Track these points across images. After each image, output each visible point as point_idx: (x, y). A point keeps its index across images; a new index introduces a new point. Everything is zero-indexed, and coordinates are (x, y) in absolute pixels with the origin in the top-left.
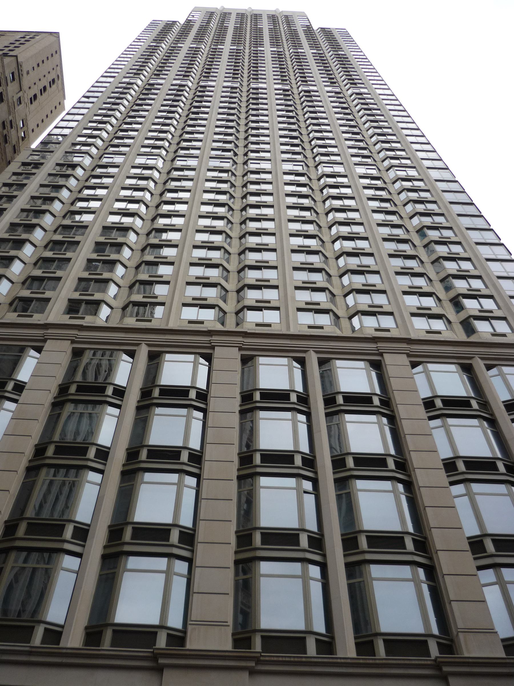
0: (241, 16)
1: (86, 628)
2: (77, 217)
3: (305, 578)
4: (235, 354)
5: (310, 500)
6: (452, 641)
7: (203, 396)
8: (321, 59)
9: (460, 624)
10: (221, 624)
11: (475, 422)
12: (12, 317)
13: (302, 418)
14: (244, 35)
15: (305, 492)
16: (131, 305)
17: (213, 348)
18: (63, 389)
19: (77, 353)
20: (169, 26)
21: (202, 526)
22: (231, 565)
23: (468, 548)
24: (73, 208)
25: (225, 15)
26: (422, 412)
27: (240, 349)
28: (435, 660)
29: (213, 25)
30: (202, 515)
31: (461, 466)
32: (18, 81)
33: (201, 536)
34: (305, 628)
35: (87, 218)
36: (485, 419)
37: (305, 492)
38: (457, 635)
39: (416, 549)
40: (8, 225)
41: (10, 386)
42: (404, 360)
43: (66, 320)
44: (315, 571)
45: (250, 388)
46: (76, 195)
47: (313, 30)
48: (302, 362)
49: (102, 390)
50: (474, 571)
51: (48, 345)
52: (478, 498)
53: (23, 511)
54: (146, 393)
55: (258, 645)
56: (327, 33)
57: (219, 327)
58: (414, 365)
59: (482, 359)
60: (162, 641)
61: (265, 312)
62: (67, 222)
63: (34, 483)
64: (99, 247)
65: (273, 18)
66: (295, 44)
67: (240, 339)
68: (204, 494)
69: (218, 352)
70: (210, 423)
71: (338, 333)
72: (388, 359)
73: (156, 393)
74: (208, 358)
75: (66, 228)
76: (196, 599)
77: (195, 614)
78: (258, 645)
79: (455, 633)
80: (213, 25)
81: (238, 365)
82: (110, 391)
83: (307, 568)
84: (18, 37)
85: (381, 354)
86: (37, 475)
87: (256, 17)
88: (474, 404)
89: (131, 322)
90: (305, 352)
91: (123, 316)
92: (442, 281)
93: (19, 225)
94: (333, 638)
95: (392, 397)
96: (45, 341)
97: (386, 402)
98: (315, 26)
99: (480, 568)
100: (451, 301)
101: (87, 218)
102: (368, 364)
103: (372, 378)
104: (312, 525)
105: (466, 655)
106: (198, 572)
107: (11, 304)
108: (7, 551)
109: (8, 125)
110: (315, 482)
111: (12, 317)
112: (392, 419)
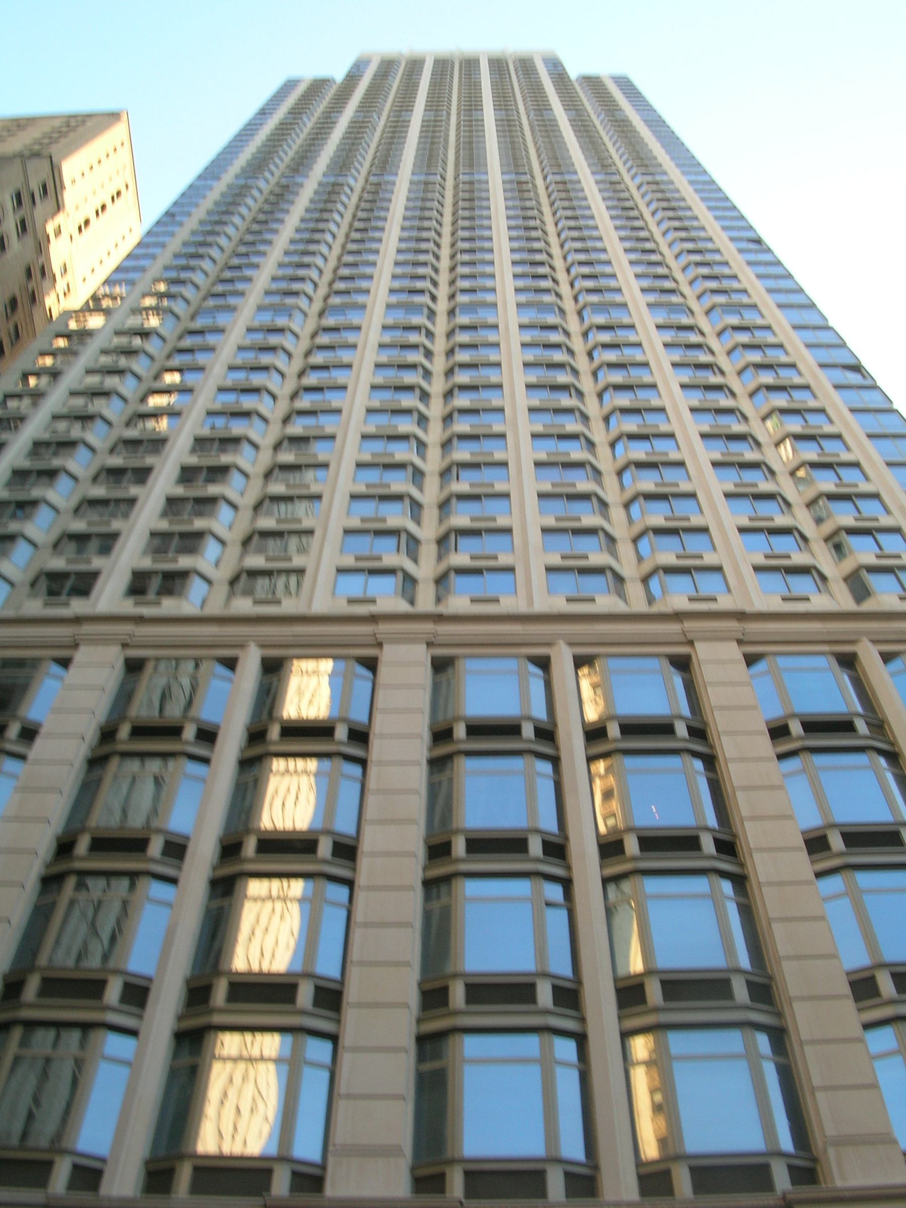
0: (443, 66)
1: (147, 1163)
2: (151, 424)
3: (547, 1064)
4: (421, 655)
5: (557, 919)
6: (815, 1160)
7: (360, 736)
8: (583, 128)
9: (830, 1130)
10: (389, 1151)
11: (861, 759)
12: (35, 607)
13: (546, 767)
14: (446, 103)
15: (548, 904)
16: (244, 577)
17: (380, 645)
18: (107, 734)
19: (134, 667)
20: (318, 86)
21: (355, 975)
22: (412, 1045)
23: (847, 990)
24: (142, 409)
25: (415, 66)
26: (765, 746)
27: (429, 644)
28: (784, 1197)
29: (396, 83)
30: (355, 954)
31: (836, 842)
32: (54, 195)
33: (351, 994)
34: (546, 1152)
35: (163, 424)
36: (880, 752)
37: (548, 904)
38: (825, 1150)
39: (752, 998)
40: (30, 445)
41: (13, 730)
42: (734, 652)
43: (129, 607)
44: (566, 1049)
45: (449, 715)
46: (147, 384)
47: (570, 81)
48: (543, 663)
49: (175, 731)
50: (858, 1031)
51: (81, 655)
52: (867, 899)
53: (35, 954)
54: (256, 735)
55: (456, 1184)
56: (593, 83)
57: (403, 606)
58: (751, 660)
59: (874, 642)
60: (281, 1185)
61: (488, 576)
62: (132, 433)
63: (52, 906)
64: (187, 474)
65: (498, 65)
66: (539, 105)
67: (429, 627)
68: (359, 916)
69: (389, 655)
70: (372, 784)
71: (620, 607)
72: (703, 652)
73: (274, 732)
74: (371, 664)
75: (132, 444)
76: (342, 1107)
77: (340, 1136)
78: (456, 1184)
79: (820, 1144)
80: (396, 83)
81: (425, 674)
82: (189, 732)
83: (551, 1046)
84: (56, 123)
85: (691, 643)
86: (59, 890)
87: (470, 65)
88: (861, 726)
89: (243, 606)
90: (549, 644)
91: (232, 593)
92: (811, 504)
93: (47, 444)
94: (596, 1167)
95: (710, 719)
96: (76, 646)
97: (699, 732)
98: (574, 71)
99: (867, 1026)
100: (826, 540)
101: (163, 424)
102: (666, 663)
103: (674, 689)
104: (562, 966)
105: (839, 1183)
106: (347, 1059)
107: (33, 584)
108: (3, 1027)
109: (36, 273)
110: (567, 884)
111: (35, 607)
112: (710, 761)
